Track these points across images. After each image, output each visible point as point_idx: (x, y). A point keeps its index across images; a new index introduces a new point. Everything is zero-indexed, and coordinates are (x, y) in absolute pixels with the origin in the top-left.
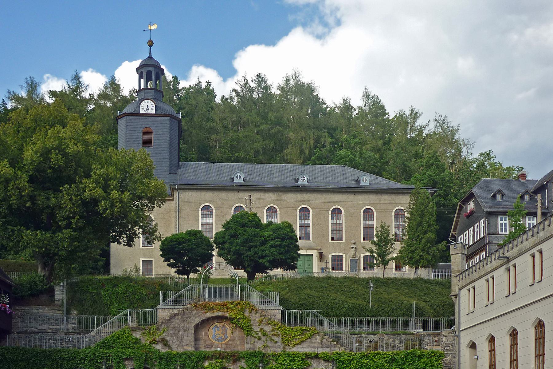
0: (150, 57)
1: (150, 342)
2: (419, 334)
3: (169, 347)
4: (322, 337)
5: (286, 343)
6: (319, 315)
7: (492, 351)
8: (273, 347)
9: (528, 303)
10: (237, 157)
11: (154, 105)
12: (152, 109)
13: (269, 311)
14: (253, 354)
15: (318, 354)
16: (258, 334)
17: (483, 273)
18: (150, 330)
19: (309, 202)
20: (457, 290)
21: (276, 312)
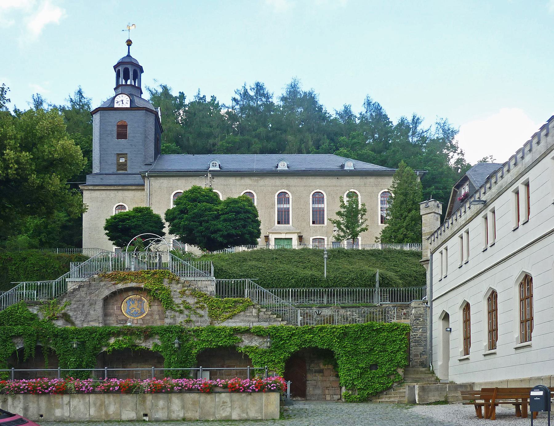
0: (129, 56)
1: (49, 318)
2: (383, 306)
3: (73, 324)
4: (259, 310)
5: (214, 317)
6: (258, 286)
7: (467, 321)
8: (198, 322)
9: (510, 254)
12: (127, 103)
14: (168, 330)
15: (250, 329)
16: (179, 307)
17: (456, 228)
19: (288, 187)
20: (429, 255)
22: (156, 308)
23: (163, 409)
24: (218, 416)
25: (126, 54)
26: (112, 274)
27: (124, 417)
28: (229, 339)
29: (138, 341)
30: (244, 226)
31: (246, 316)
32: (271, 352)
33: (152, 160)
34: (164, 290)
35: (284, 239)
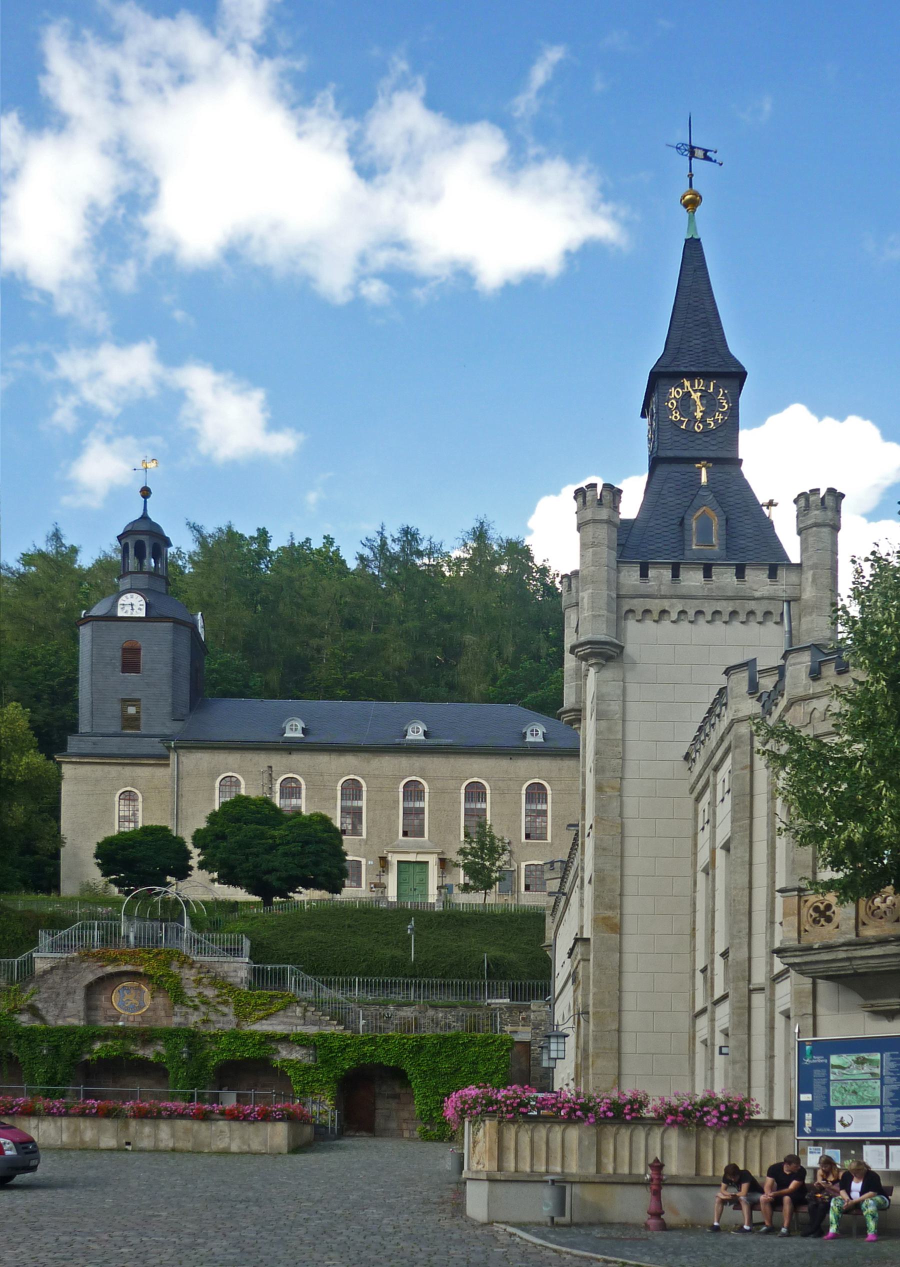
0: (145, 517)
1: (9, 1010)
3: (42, 1019)
5: (242, 1016)
8: (219, 1022)
10: (352, 679)
11: (143, 602)
12: (140, 609)
13: (226, 965)
15: (288, 1035)
16: (193, 1001)
18: (9, 991)
21: (239, 969)
22: (160, 1000)
23: (149, 1136)
24: (214, 1148)
25: (138, 514)
26: (98, 953)
27: (103, 1145)
28: (259, 1049)
29: (132, 1047)
30: (316, 864)
31: (287, 1017)
32: (317, 1068)
33: (185, 711)
34: (171, 976)
35: (414, 862)
